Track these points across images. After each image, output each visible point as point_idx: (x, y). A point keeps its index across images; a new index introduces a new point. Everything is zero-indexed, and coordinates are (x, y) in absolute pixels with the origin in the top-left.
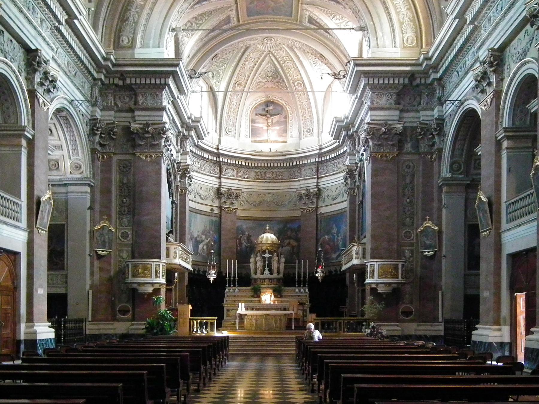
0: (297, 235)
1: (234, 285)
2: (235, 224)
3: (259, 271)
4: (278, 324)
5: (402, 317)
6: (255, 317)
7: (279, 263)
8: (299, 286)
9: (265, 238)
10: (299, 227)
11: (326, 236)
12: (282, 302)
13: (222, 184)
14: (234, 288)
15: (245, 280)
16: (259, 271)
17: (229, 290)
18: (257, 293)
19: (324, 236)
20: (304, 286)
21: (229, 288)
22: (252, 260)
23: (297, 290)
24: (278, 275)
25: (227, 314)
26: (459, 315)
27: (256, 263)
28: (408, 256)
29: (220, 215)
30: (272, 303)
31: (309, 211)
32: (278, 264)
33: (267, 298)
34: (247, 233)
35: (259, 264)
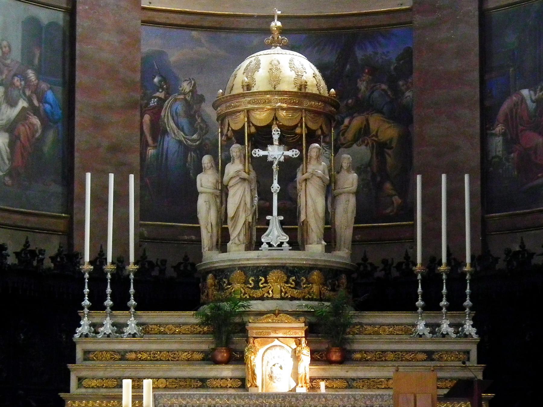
0: (397, 92)
1: (120, 304)
7: (330, 190)
8: (432, 306)
10: (408, 55)
11: (525, 92)
12: (350, 383)
15: (172, 280)
16: (237, 232)
17: (95, 326)
18: (229, 339)
19: (517, 90)
20: (456, 306)
22: (206, 181)
23: (421, 327)
27: (222, 192)
30: (302, 390)
32: (328, 190)
34: (186, 87)
35: (241, 199)
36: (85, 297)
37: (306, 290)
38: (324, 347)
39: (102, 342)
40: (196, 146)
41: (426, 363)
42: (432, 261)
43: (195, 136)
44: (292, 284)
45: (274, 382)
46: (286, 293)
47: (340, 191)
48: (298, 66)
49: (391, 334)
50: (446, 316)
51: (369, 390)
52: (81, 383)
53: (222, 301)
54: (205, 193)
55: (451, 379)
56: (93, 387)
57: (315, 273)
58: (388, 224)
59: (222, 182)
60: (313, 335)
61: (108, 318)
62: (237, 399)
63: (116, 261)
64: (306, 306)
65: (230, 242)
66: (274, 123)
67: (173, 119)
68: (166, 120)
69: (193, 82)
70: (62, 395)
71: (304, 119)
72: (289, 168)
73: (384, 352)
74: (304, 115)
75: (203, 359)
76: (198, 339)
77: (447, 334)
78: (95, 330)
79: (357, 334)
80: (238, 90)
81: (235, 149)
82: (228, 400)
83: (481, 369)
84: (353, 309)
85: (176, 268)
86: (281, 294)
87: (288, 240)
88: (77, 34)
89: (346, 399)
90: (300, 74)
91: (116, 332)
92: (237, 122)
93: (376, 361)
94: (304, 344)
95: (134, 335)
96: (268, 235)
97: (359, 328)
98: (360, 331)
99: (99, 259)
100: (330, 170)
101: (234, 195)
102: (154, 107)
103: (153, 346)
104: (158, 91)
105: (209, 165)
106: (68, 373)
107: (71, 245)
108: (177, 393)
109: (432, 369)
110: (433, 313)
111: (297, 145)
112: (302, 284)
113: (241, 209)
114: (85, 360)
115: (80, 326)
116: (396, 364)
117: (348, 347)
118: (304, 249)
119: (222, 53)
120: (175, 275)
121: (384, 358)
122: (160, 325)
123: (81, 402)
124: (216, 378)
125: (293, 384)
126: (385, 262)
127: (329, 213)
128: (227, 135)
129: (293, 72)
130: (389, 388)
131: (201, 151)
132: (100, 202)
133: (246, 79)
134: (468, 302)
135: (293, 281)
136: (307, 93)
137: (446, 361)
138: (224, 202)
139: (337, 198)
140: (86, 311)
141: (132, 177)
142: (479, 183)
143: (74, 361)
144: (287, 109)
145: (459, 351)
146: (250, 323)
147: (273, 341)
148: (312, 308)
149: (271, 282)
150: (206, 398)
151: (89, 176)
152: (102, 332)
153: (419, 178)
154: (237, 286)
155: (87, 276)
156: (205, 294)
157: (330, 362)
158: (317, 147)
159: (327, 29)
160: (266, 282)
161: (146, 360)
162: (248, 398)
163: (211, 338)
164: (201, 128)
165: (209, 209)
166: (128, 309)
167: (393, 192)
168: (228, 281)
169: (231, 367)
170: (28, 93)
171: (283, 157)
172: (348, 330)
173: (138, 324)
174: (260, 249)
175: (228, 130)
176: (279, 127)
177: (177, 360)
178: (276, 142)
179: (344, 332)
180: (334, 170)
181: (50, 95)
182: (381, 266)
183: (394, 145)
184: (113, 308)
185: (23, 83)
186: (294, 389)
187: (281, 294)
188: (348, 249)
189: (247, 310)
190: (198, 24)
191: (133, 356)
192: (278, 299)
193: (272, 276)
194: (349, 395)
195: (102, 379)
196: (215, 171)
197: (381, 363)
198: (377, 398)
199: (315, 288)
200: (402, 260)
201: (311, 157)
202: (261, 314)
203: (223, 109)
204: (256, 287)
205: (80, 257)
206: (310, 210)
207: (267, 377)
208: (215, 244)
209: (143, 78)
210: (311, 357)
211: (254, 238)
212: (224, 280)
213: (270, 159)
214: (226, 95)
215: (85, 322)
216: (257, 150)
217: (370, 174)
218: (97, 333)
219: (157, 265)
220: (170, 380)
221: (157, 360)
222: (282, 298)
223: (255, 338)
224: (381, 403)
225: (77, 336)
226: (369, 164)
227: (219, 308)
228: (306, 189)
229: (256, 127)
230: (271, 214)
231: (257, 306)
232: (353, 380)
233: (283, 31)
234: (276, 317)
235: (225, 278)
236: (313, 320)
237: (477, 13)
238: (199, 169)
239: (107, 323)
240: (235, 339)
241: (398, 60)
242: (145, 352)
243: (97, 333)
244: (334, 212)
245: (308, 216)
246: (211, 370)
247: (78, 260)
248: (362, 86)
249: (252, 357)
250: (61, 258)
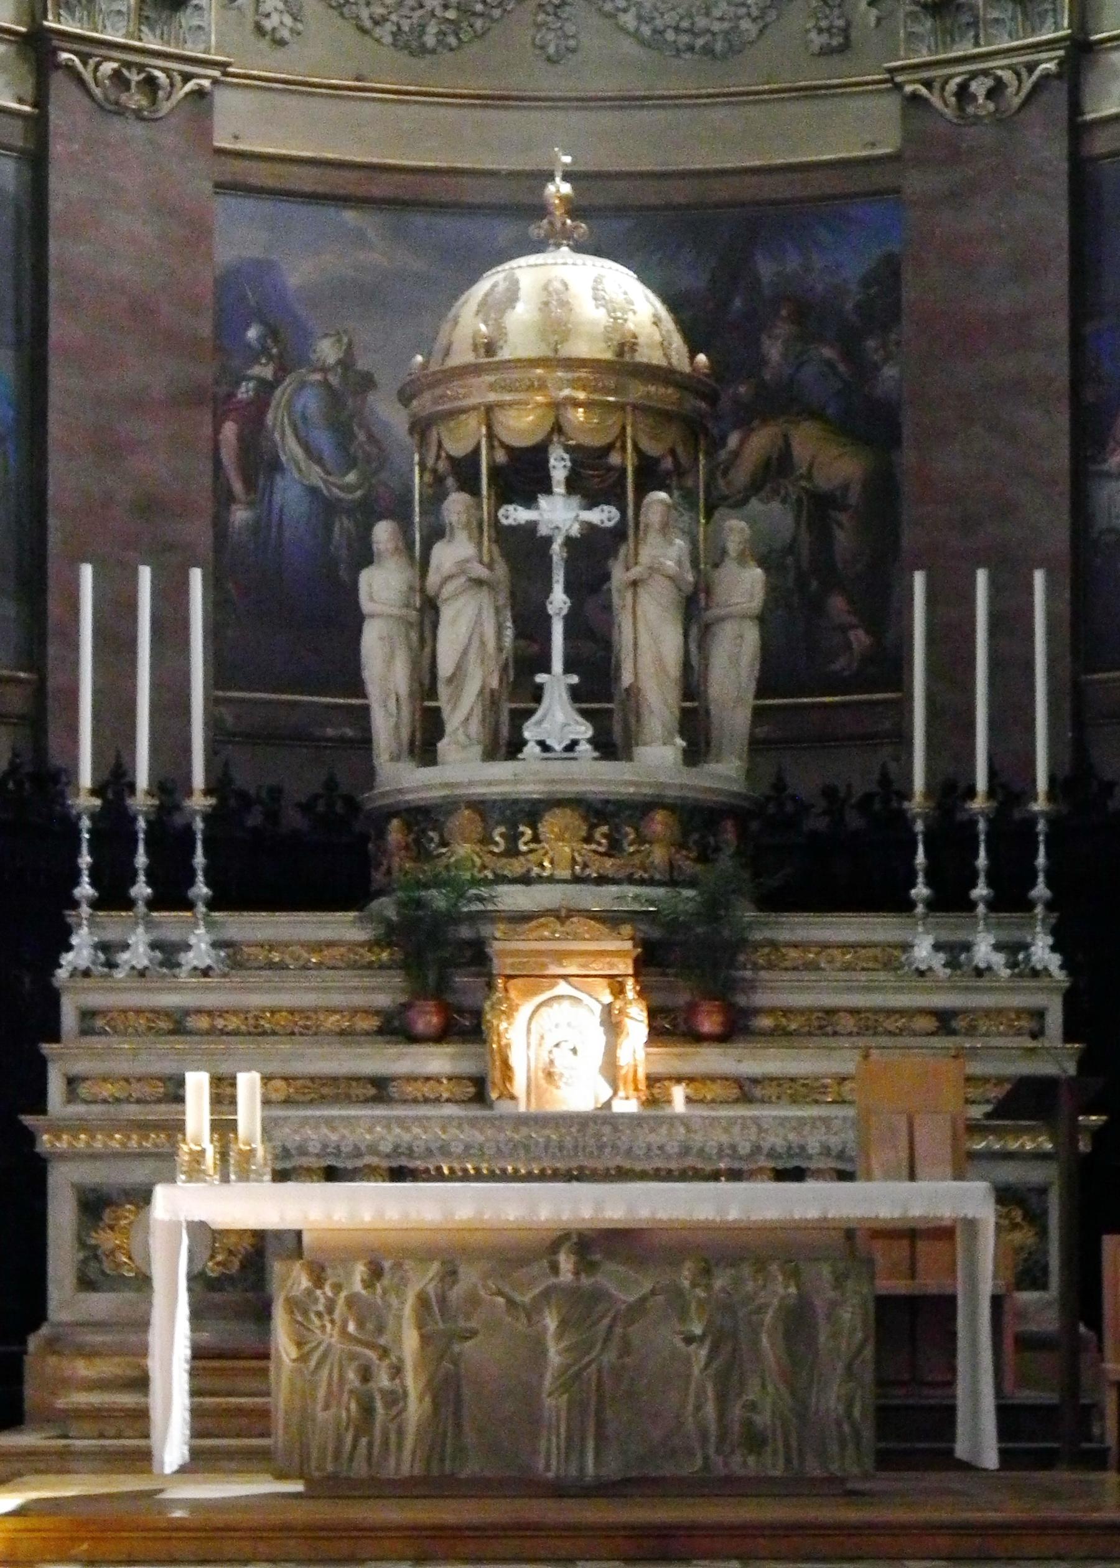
0: (863, 370)
1: (171, 895)
2: (198, 234)
3: (463, 713)
4: (764, 1397)
6: (423, 1280)
7: (695, 609)
8: (951, 899)
9: (522, 314)
10: (888, 275)
12: (746, 1090)
14: (171, 923)
15: (299, 835)
16: (463, 713)
17: (108, 949)
18: (446, 981)
20: (1010, 898)
21: (114, 926)
22: (382, 586)
23: (923, 951)
24: (694, 755)
25: (91, 1254)
27: (427, 611)
29: (38, 124)
30: (627, 1105)
31: (996, 91)
33: (572, 1038)
34: (328, 351)
35: (471, 630)
36: (1036, 877)
37: (637, 860)
38: (682, 999)
39: (129, 989)
40: (353, 501)
41: (936, 1041)
42: (951, 790)
43: (351, 478)
44: (599, 844)
45: (558, 1087)
46: (585, 866)
47: (722, 612)
48: (614, 296)
49: (847, 968)
50: (986, 924)
51: (795, 1107)
52: (75, 1089)
53: (426, 886)
54: (380, 616)
55: (1000, 1080)
56: (105, 1101)
57: (659, 816)
58: (837, 699)
59: (423, 590)
60: (653, 969)
61: (141, 930)
62: (466, 1126)
63: (155, 790)
64: (636, 898)
65: (445, 740)
66: (555, 439)
67: (297, 436)
68: (277, 436)
69: (345, 340)
70: (28, 1120)
71: (629, 429)
72: (593, 554)
73: (831, 1012)
74: (629, 420)
75: (380, 1031)
76: (367, 982)
77: (989, 968)
78: (107, 960)
79: (763, 968)
80: (462, 356)
81: (456, 505)
82: (444, 1129)
83: (1073, 1054)
84: (752, 906)
85: (305, 808)
86: (573, 869)
87: (590, 733)
88: (51, 215)
89: (736, 1130)
90: (619, 314)
91: (162, 964)
92: (462, 438)
93: (810, 1034)
94: (630, 994)
95: (206, 972)
96: (539, 723)
97: (768, 954)
98: (769, 961)
99: (115, 781)
100: (695, 563)
101: (454, 622)
102: (250, 403)
103: (259, 996)
104: (255, 360)
105: (390, 546)
106: (40, 1066)
107: (40, 748)
108: (318, 1113)
109: (953, 1052)
110: (951, 918)
111: (611, 494)
112: (625, 844)
113: (472, 656)
114: (85, 1032)
115: (69, 948)
116: (861, 1042)
117: (741, 1000)
118: (629, 758)
119: (418, 265)
121: (829, 1029)
122: (272, 947)
123: (76, 1138)
124: (411, 1079)
125: (606, 1092)
126: (829, 792)
127: (692, 667)
128: (434, 471)
129: (603, 311)
130: (844, 1102)
131: (368, 512)
132: (115, 643)
133: (483, 328)
134: (1040, 890)
135: (605, 836)
136: (640, 364)
137: (986, 1035)
138: (429, 642)
139: (715, 629)
140: (85, 910)
141: (196, 576)
142: (1067, 595)
143: (55, 1036)
144: (587, 405)
145: (1020, 1012)
146: (496, 939)
147: (552, 986)
148: (651, 902)
149: (548, 841)
150: (388, 1127)
151: (87, 572)
152: (126, 962)
153: (919, 580)
154: (463, 849)
155: (86, 823)
156: (383, 868)
157: (698, 1038)
158: (662, 502)
159: (688, 206)
160: (536, 839)
161: (236, 1033)
162: (493, 1125)
163: (397, 979)
164: (368, 459)
165: (392, 656)
166: (189, 906)
167: (854, 620)
168: (442, 836)
169: (448, 1049)
171: (576, 526)
172: (742, 958)
173: (216, 945)
174: (520, 756)
175: (438, 457)
176: (568, 449)
177: (316, 1034)
178: (559, 489)
179: (732, 964)
180: (706, 559)
182: (821, 804)
183: (853, 498)
184: (153, 904)
186: (608, 1104)
187: (573, 869)
188: (740, 758)
189: (490, 907)
190: (361, 191)
191: (203, 1023)
192: (565, 881)
193: (551, 824)
194: (743, 1117)
195: (127, 1080)
196: (404, 561)
197: (824, 1040)
198: (814, 1126)
199: (659, 855)
200: (874, 788)
201: (647, 526)
202: (522, 918)
203: (424, 404)
204: (512, 852)
205: (64, 779)
206: (646, 659)
207: (541, 1074)
208: (405, 747)
209: (219, 328)
210: (650, 1026)
211: (505, 731)
212: (431, 834)
213: (543, 531)
214: (434, 367)
215: (82, 939)
216: (511, 508)
217: (792, 575)
218: (111, 965)
220: (300, 1083)
221: (264, 1033)
222: (577, 880)
223: (510, 977)
224: (824, 1138)
225: (62, 974)
226: (791, 548)
227: (419, 904)
228: (634, 608)
229: (510, 450)
230: (547, 670)
231: (513, 898)
232: (755, 1081)
233: (575, 210)
234: (563, 923)
235: (434, 830)
236: (656, 933)
237: (1065, 166)
238: (365, 557)
239: (137, 943)
240: (461, 979)
241: (866, 282)
242: (235, 1012)
243: (111, 965)
244: (707, 666)
245: (642, 676)
246: (400, 1057)
247: (59, 787)
248: (774, 351)
249: (503, 1025)
250: (15, 782)
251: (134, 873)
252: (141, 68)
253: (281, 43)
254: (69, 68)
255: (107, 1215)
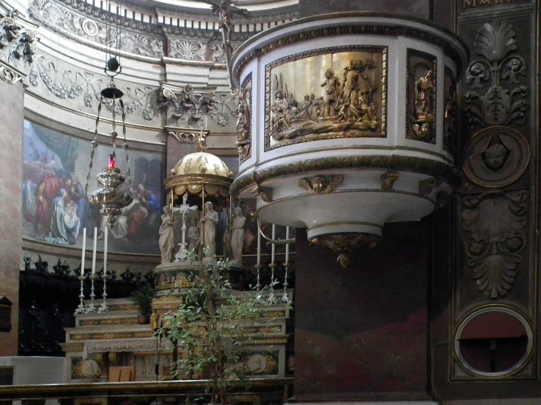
1: (99, 296)
5: (464, 370)
13: (169, 77)
26: (451, 85)
28: (496, 53)
29: (165, 147)
85: (122, 275)
106: (64, 332)
110: (279, 290)
114: (81, 325)
115: (78, 308)
120: (121, 279)
145: (279, 311)
170: (139, 196)
181: (153, 196)
185: (136, 191)
219: (136, 275)
229: (178, 195)
230: (181, 242)
242: (110, 319)
251: (91, 291)
252: (188, 133)
253: (223, 126)
254: (172, 135)
255: (78, 363)
